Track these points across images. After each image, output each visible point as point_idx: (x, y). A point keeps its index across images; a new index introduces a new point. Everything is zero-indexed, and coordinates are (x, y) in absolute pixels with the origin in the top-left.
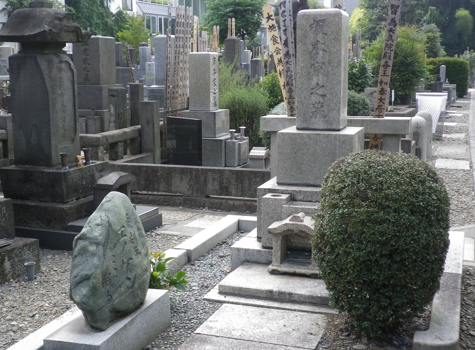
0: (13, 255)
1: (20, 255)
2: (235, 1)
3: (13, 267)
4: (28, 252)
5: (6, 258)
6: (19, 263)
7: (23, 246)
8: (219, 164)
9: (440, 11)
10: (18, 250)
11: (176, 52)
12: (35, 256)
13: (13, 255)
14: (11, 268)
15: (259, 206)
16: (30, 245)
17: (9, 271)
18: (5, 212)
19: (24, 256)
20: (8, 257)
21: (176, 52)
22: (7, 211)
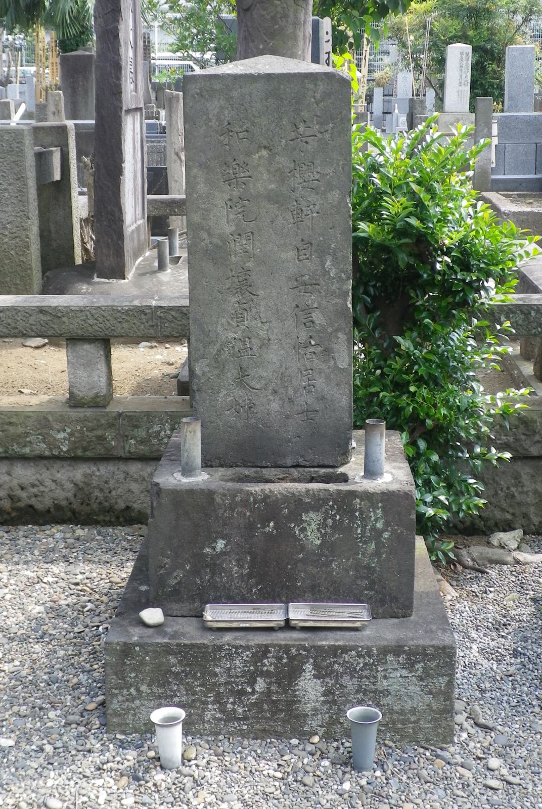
0: (336, 667)
1: (366, 673)
2: (294, 782)
3: (334, 702)
4: (404, 673)
5: (309, 667)
6: (360, 696)
7: (385, 651)
8: (289, 53)
9: (430, 329)
10: (360, 655)
11: (462, 57)
12: (430, 693)
13: (336, 667)
14: (324, 702)
15: (58, 241)
16: (410, 653)
17: (315, 710)
18: (379, 525)
19: (385, 683)
20: (316, 666)
21: (462, 57)
22: (387, 524)
